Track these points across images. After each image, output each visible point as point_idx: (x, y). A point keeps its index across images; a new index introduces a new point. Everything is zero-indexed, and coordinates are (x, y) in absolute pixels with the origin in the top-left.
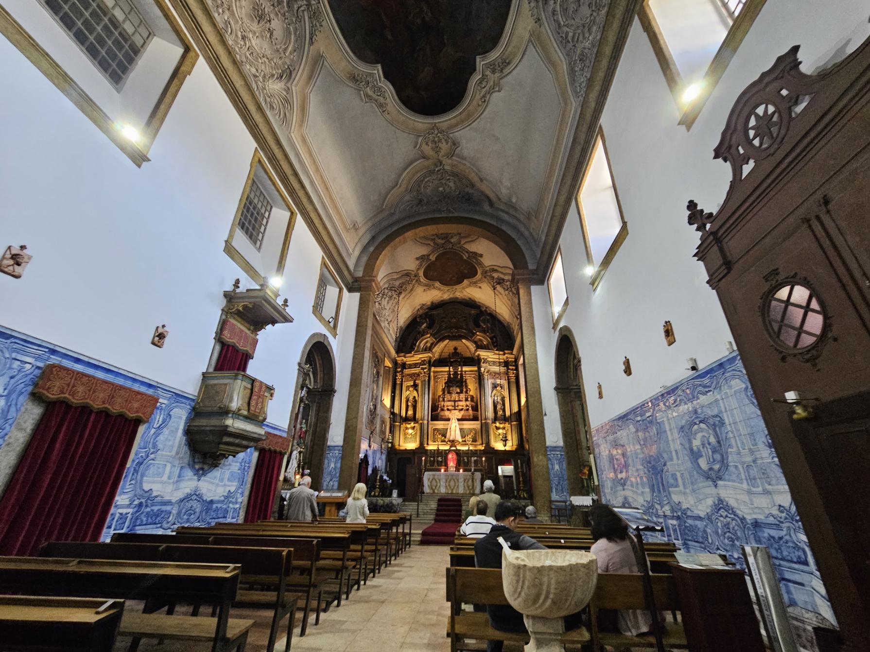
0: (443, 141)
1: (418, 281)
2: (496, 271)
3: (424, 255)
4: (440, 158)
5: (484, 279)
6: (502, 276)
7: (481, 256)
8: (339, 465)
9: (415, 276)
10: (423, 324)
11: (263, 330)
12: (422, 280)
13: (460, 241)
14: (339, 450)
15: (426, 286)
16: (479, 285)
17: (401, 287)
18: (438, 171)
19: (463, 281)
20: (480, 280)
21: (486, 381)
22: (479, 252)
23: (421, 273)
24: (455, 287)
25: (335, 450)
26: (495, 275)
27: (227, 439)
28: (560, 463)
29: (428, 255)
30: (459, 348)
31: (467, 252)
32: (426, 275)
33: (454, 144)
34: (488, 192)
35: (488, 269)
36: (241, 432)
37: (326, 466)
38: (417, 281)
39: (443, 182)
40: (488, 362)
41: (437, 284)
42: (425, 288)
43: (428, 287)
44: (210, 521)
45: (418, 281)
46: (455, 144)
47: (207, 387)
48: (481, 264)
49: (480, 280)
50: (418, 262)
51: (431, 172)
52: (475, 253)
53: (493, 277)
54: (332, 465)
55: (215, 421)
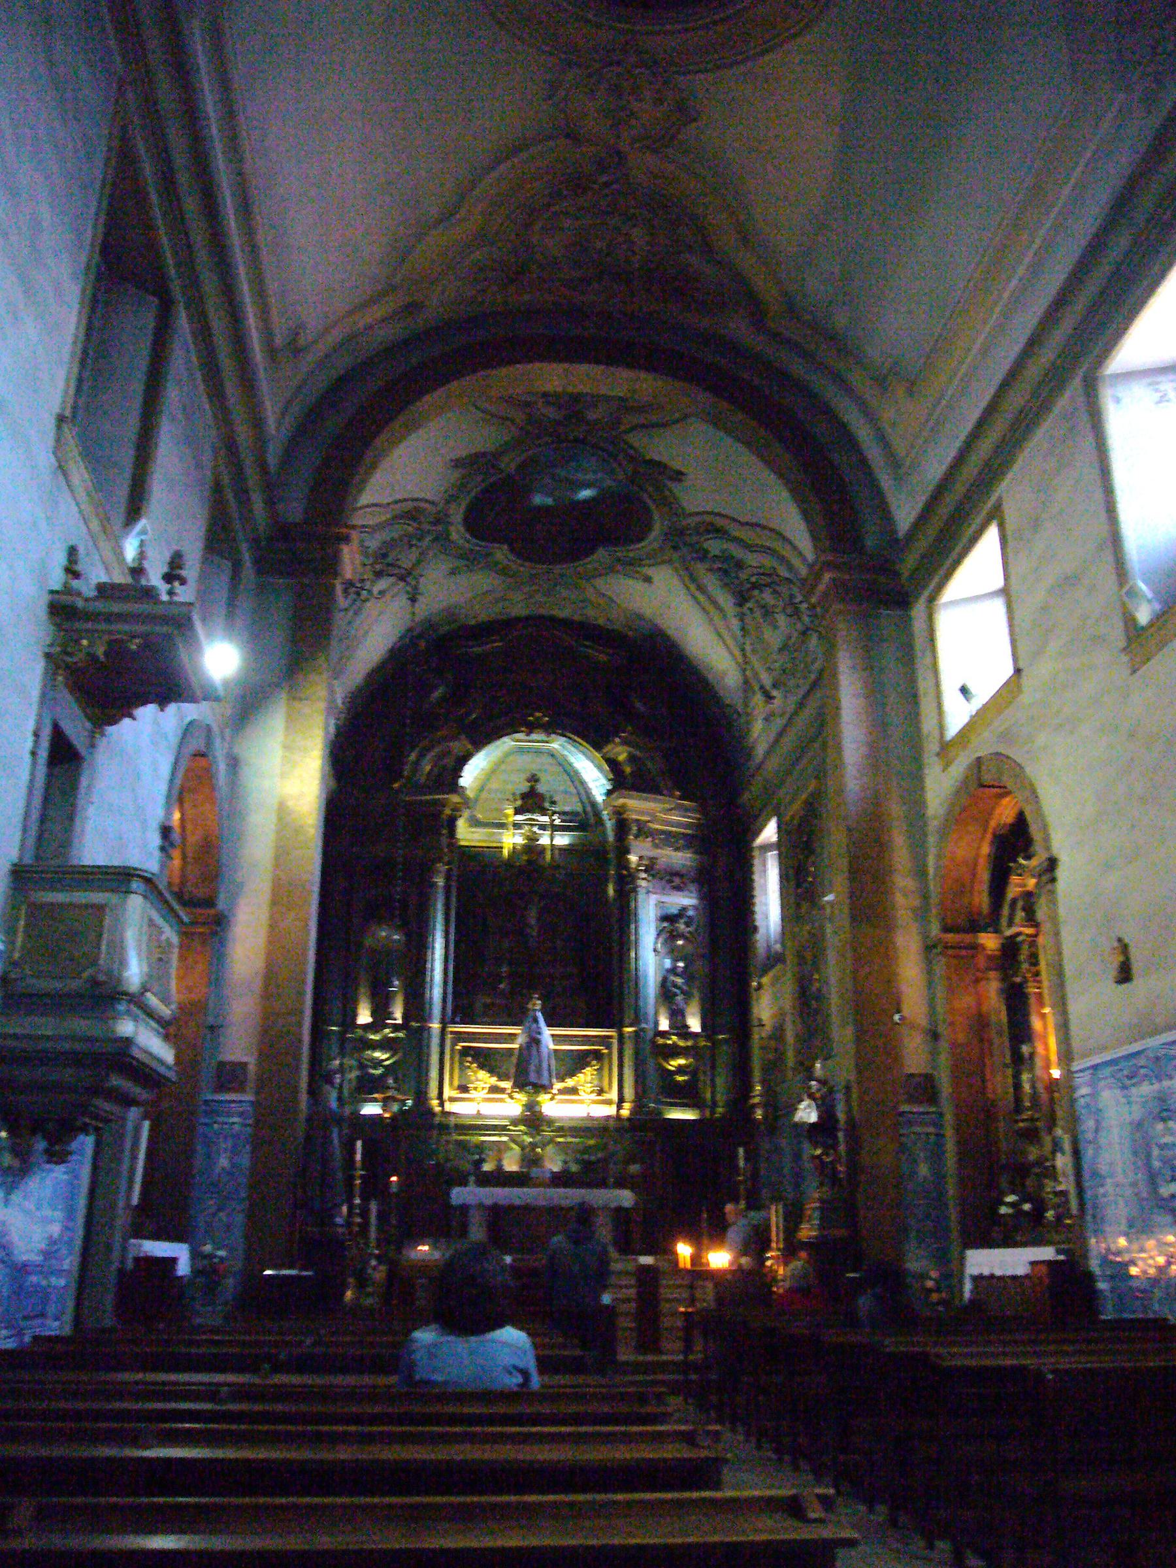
0: (647, 95)
1: (442, 539)
2: (720, 532)
3: (484, 454)
4: (623, 146)
5: (669, 553)
6: (737, 552)
7: (679, 476)
8: (245, 1161)
9: (437, 522)
10: (435, 688)
11: (126, 721)
12: (454, 536)
13: (619, 421)
14: (241, 1115)
15: (460, 557)
16: (649, 571)
17: (385, 556)
18: (607, 185)
19: (592, 551)
20: (649, 556)
21: (641, 896)
22: (676, 465)
23: (457, 514)
24: (558, 569)
25: (228, 1115)
26: (714, 546)
27: (116, 1081)
28: (234, 1152)
29: (497, 455)
30: (544, 778)
31: (632, 459)
32: (472, 522)
33: (681, 108)
34: (762, 283)
35: (692, 521)
36: (147, 1060)
37: (199, 1162)
38: (436, 539)
39: (614, 221)
40: (652, 834)
41: (501, 553)
42: (460, 563)
43: (470, 560)
44: (23, 1323)
45: (442, 539)
46: (685, 113)
47: (35, 910)
48: (669, 504)
49: (649, 556)
50: (456, 474)
51: (578, 184)
52: (661, 467)
53: (706, 552)
54: (224, 1162)
55: (80, 1025)
